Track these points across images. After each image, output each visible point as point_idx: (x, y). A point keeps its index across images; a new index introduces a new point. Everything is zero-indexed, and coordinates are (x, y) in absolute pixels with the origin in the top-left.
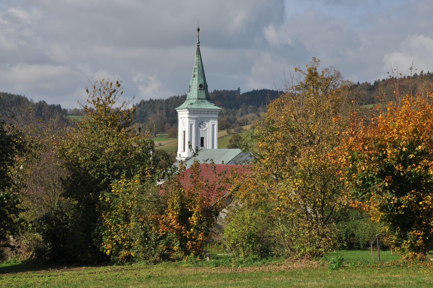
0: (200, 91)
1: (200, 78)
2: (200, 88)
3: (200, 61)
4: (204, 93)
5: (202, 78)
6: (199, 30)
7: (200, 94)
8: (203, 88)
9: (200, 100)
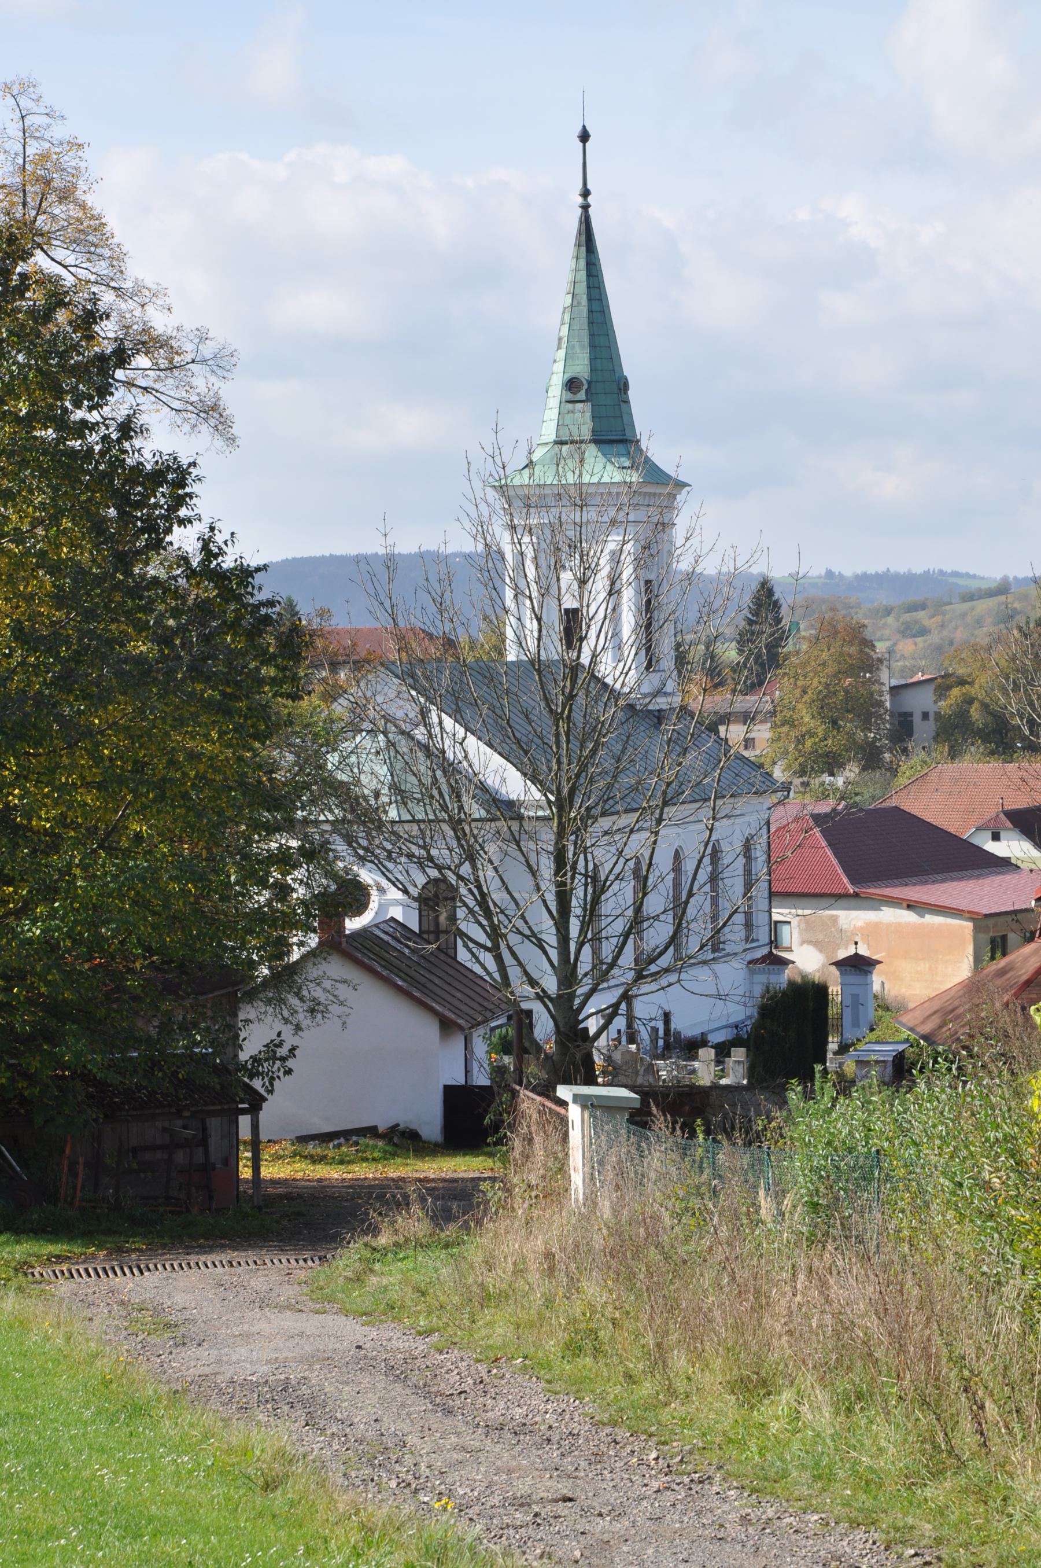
0: (570, 406)
1: (578, 349)
2: (570, 396)
3: (582, 275)
4: (588, 415)
5: (582, 347)
6: (584, 137)
7: (568, 419)
8: (582, 395)
9: (565, 448)
